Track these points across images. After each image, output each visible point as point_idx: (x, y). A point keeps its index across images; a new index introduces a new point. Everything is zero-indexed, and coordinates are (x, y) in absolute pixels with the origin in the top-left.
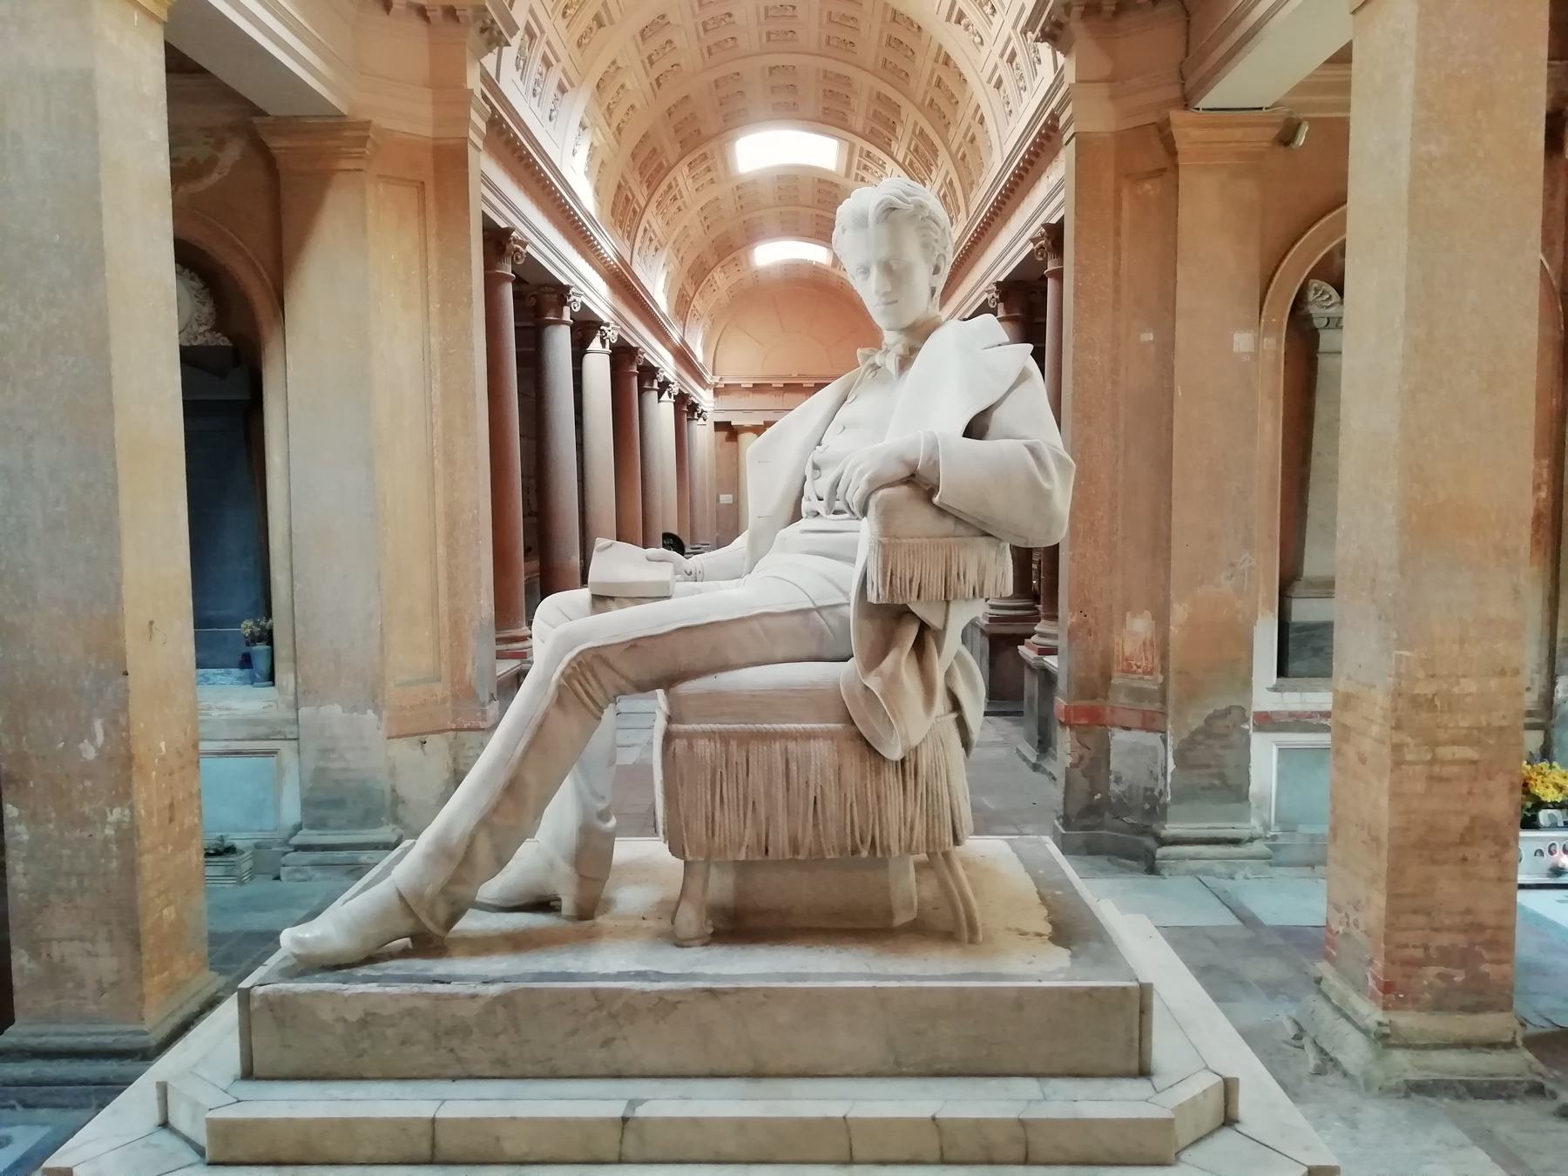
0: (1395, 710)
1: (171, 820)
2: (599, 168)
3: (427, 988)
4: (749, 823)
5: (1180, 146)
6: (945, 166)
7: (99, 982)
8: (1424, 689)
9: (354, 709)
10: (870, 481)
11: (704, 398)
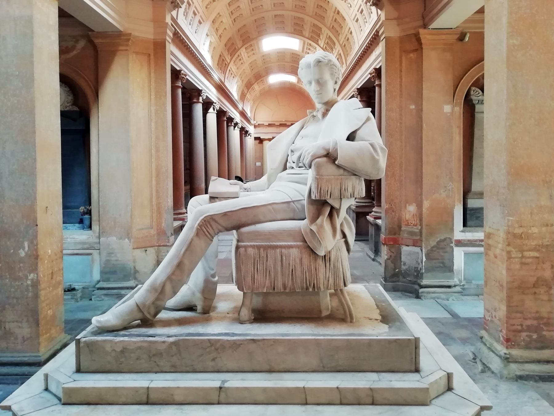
1: (52, 278)
7: (23, 337)
8: (518, 231)
9: (121, 238)
10: (312, 156)
11: (250, 129)
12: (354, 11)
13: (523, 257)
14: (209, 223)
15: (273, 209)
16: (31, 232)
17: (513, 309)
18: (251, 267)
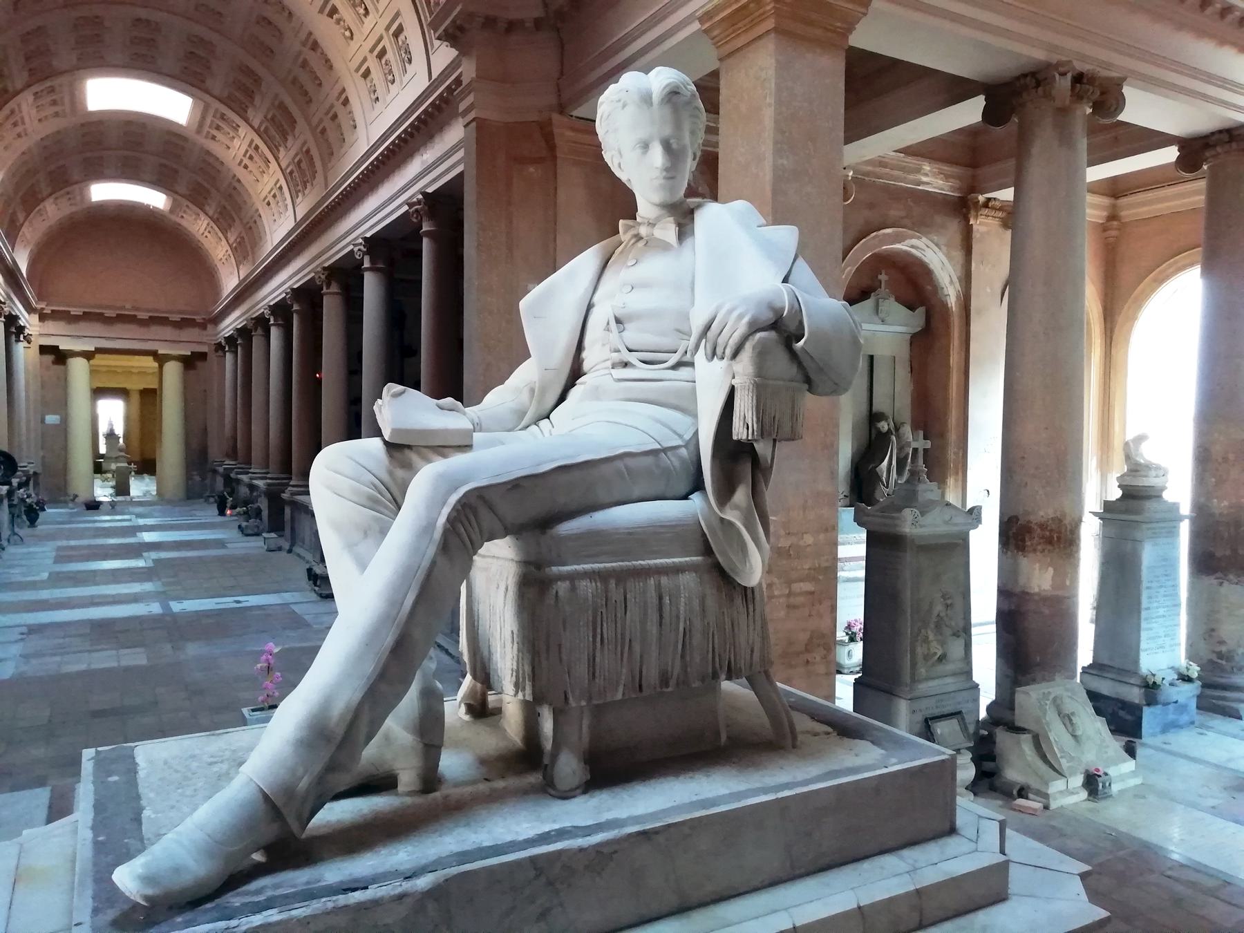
3: (342, 900)
4: (625, 659)
5: (558, 141)
6: (303, 134)
11: (29, 322)
12: (360, 48)
13: (790, 595)
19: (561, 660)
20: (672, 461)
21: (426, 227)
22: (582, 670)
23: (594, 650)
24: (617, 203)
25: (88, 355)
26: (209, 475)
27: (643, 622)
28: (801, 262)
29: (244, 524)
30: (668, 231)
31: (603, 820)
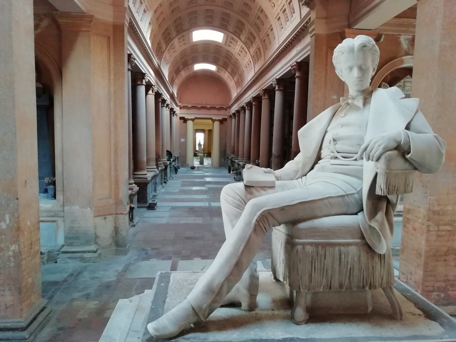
0: (428, 215)
1: (31, 248)
2: (153, 37)
6: (257, 43)
7: (6, 305)
8: (437, 208)
9: (83, 207)
10: (384, 148)
11: (177, 109)
12: (277, 10)
13: (438, 231)
14: (267, 218)
15: (329, 202)
16: (11, 205)
17: (428, 273)
18: (308, 266)
19: (298, 274)
20: (351, 200)
21: (297, 74)
22: (306, 279)
23: (312, 271)
24: (341, 88)
25: (193, 120)
26: (226, 159)
27: (333, 263)
28: (420, 114)
29: (236, 177)
30: (359, 102)
31: (309, 337)
